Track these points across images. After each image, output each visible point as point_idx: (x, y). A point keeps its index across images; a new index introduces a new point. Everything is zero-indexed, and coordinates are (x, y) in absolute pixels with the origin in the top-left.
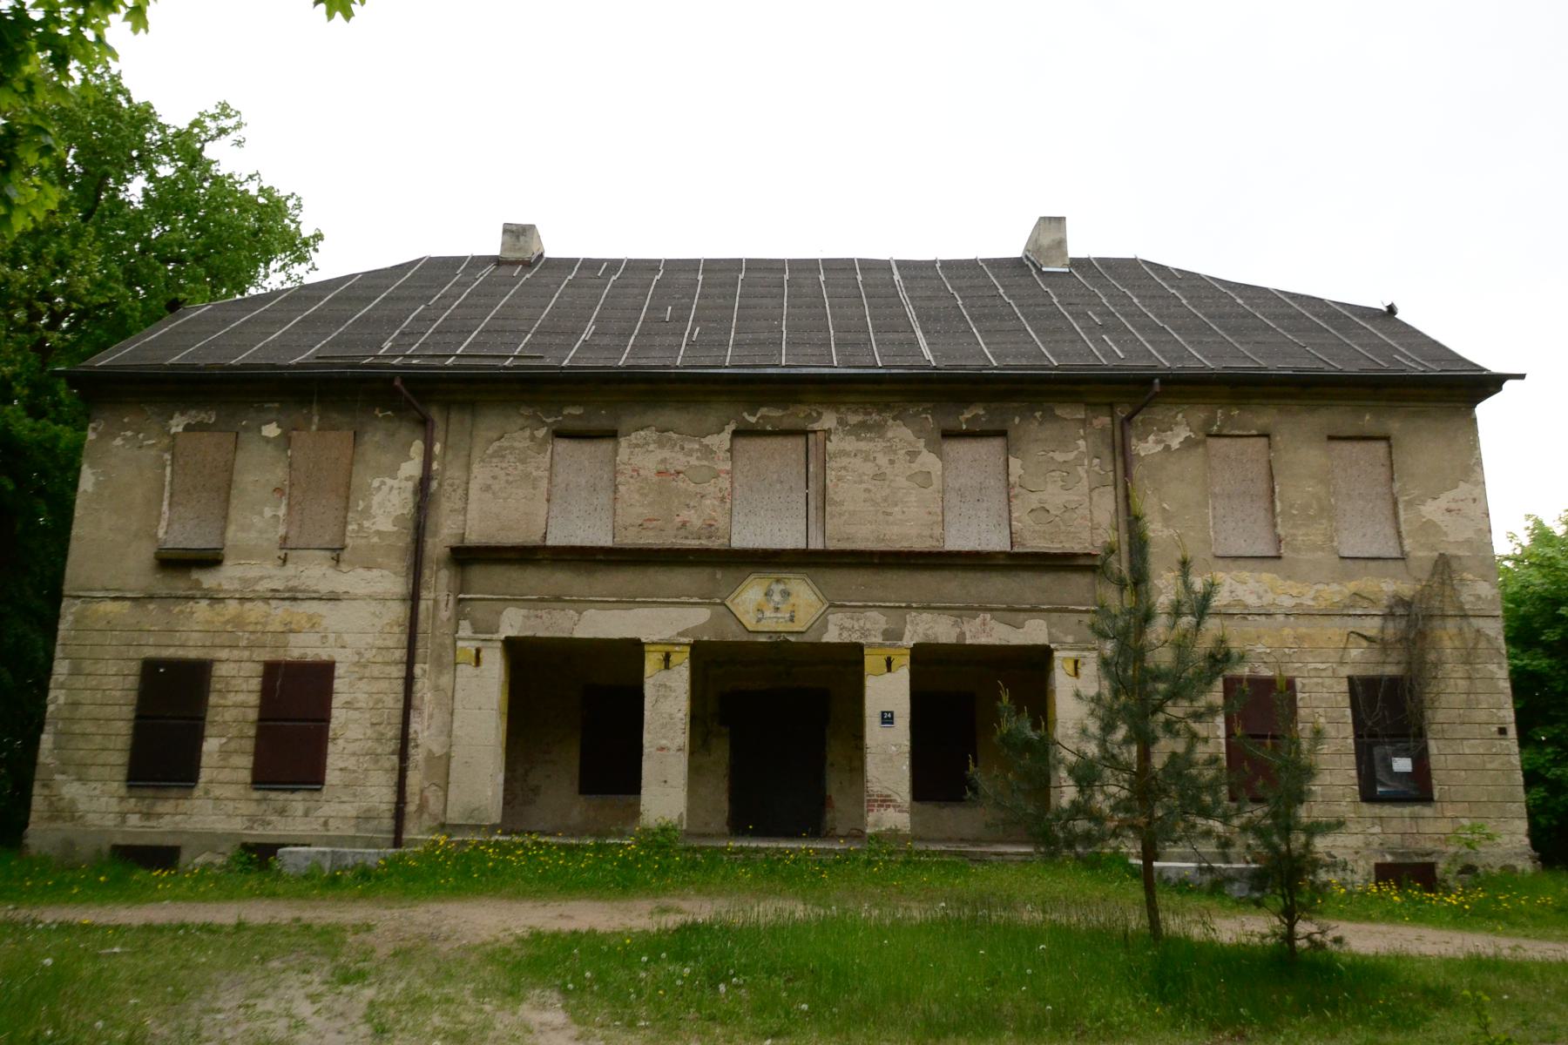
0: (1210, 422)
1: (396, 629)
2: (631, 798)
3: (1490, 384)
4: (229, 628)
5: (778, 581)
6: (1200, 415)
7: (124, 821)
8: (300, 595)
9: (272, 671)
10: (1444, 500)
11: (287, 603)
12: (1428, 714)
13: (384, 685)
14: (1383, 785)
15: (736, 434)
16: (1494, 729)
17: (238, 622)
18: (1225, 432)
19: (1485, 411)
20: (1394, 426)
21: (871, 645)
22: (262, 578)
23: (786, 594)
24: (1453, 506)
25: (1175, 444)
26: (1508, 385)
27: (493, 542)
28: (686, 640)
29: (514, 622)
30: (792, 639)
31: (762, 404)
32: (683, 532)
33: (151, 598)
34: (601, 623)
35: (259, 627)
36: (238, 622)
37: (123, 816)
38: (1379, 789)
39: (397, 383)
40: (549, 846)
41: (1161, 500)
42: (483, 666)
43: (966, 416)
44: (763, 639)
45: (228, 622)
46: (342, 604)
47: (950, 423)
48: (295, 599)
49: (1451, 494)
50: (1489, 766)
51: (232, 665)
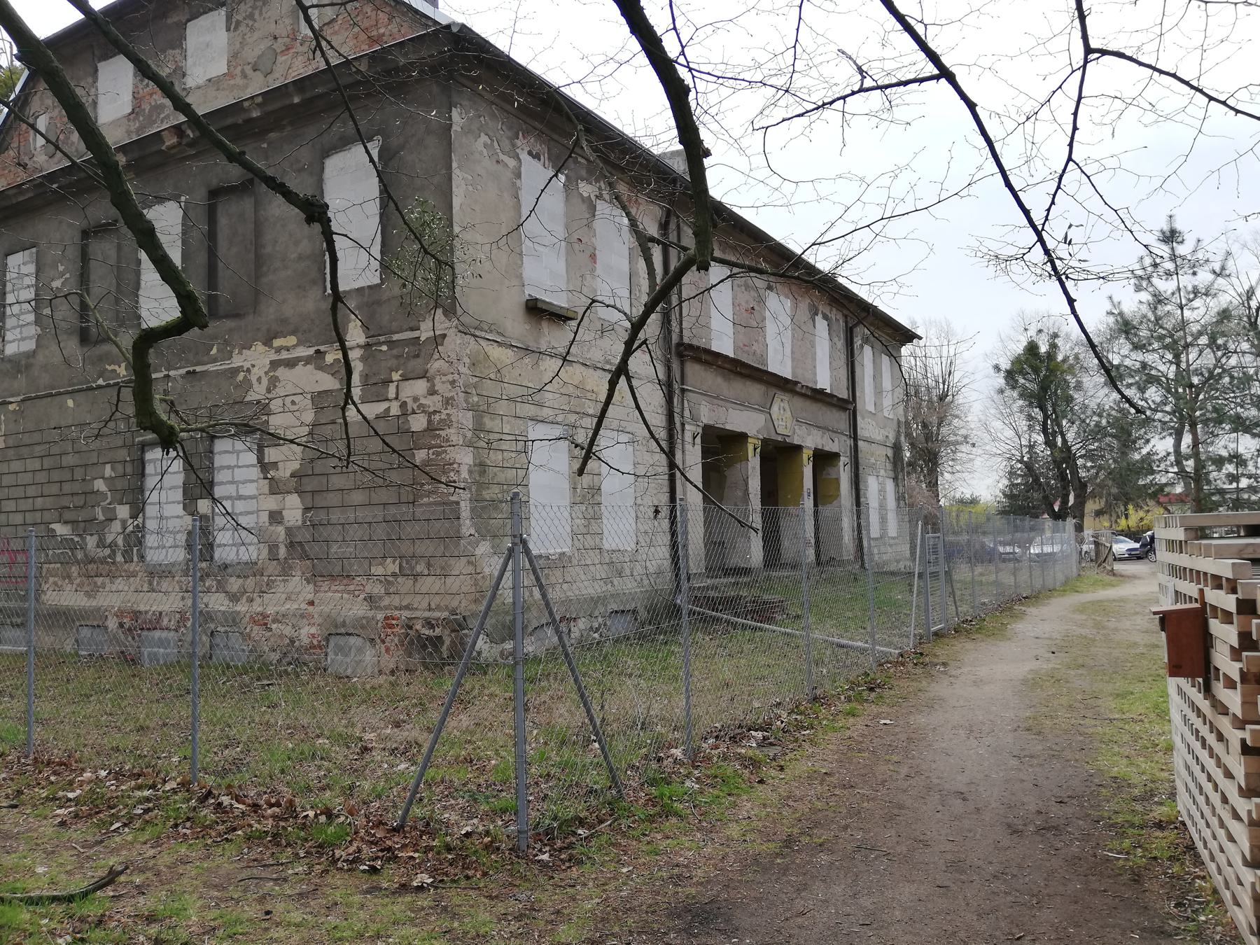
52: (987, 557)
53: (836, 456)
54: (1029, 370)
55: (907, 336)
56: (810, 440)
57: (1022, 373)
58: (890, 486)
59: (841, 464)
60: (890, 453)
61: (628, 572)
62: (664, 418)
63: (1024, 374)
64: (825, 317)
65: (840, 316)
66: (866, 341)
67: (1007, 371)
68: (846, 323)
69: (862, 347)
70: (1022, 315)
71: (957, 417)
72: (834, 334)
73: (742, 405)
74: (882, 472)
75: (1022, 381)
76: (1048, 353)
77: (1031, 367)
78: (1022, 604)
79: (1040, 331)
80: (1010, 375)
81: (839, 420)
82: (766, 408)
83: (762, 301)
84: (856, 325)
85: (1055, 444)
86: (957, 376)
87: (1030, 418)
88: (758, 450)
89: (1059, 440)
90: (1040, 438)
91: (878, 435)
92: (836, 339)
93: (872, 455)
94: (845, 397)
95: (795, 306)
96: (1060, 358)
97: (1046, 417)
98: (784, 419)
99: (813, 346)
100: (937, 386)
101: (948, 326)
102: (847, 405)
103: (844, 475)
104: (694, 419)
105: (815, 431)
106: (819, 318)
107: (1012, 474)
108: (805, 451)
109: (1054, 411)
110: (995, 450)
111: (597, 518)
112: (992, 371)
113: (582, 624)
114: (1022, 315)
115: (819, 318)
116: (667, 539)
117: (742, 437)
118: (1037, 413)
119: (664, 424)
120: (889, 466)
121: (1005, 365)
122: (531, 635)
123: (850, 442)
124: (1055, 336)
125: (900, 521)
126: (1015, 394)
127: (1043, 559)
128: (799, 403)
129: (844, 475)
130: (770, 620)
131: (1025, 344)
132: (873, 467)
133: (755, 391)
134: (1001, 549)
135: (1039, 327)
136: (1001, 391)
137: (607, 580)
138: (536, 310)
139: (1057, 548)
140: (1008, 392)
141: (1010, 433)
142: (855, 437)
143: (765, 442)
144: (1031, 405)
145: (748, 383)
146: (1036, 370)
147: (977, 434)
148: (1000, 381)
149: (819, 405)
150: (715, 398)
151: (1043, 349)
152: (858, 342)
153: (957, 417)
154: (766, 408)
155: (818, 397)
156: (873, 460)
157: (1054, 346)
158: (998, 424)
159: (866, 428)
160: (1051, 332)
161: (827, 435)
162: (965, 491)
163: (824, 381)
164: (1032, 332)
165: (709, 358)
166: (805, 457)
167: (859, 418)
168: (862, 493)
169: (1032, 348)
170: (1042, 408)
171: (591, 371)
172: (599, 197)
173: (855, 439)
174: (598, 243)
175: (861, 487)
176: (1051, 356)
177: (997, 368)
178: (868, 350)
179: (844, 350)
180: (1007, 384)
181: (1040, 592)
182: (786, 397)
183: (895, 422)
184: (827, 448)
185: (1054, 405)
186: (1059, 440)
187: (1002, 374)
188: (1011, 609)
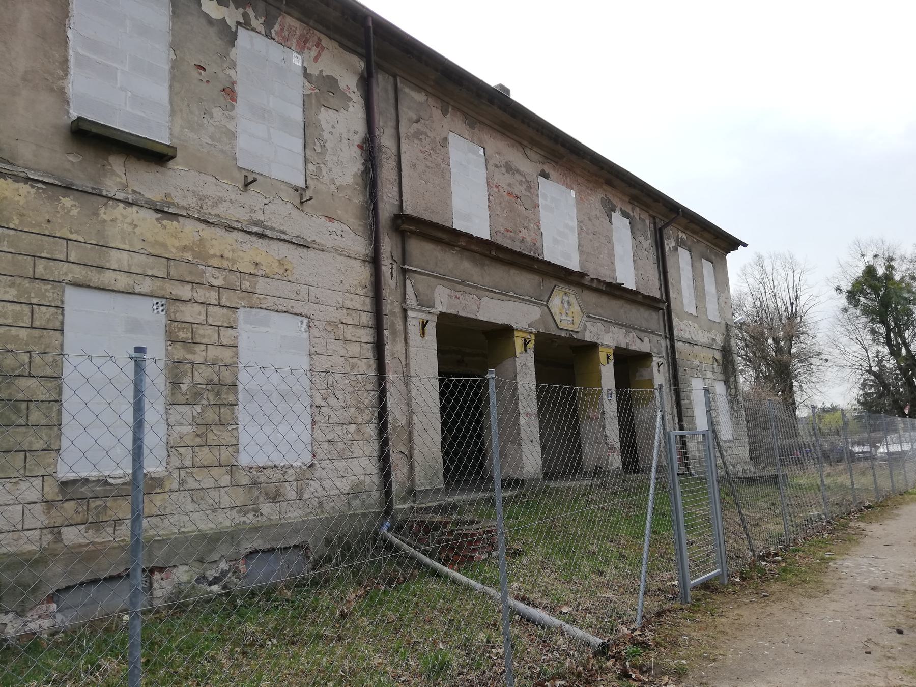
1: (360, 291)
3: (733, 244)
4: (188, 256)
7: (58, 537)
8: (268, 233)
11: (254, 238)
12: (362, 168)
13: (354, 349)
17: (200, 252)
19: (731, 257)
22: (221, 200)
26: (741, 247)
27: (427, 216)
28: (534, 330)
29: (444, 301)
33: (68, 188)
34: (493, 311)
35: (225, 264)
36: (200, 252)
37: (55, 530)
40: (552, 610)
42: (426, 338)
43: (692, 226)
44: (563, 334)
45: (185, 248)
46: (311, 253)
48: (262, 236)
51: (198, 308)
52: (834, 456)
53: (647, 357)
54: (869, 291)
55: (733, 244)
56: (609, 338)
57: (862, 291)
58: (720, 389)
59: (654, 365)
60: (718, 356)
61: (291, 494)
62: (368, 301)
63: (865, 295)
64: (625, 215)
65: (645, 216)
66: (680, 243)
67: (848, 292)
68: (655, 224)
69: (675, 249)
70: (858, 242)
71: (804, 333)
72: (638, 233)
73: (504, 294)
74: (709, 375)
75: (862, 299)
76: (885, 274)
77: (870, 286)
78: (862, 519)
79: (876, 256)
80: (852, 296)
81: (654, 320)
82: (543, 301)
83: (531, 187)
84: (666, 225)
85: (900, 354)
86: (803, 299)
87: (873, 332)
88: (531, 345)
89: (904, 352)
90: (885, 350)
91: (703, 337)
92: (642, 239)
93: (696, 357)
94: (658, 296)
95: (579, 201)
96: (897, 278)
97: (889, 331)
98: (568, 313)
99: (610, 241)
100: (787, 309)
101: (792, 258)
102: (659, 305)
103: (660, 376)
104: (425, 303)
105: (616, 329)
106: (616, 216)
107: (864, 385)
108: (601, 349)
109: (896, 325)
110: (845, 362)
111: (228, 424)
112: (834, 292)
113: (182, 574)
114: (858, 242)
115: (616, 216)
116: (373, 448)
117: (505, 332)
118: (882, 329)
119: (369, 307)
120: (717, 369)
121: (847, 286)
122: (51, 599)
123: (664, 343)
124: (891, 259)
125: (736, 425)
126: (858, 312)
127: (894, 459)
128: (592, 298)
129: (660, 376)
130: (465, 561)
131: (863, 268)
132: (697, 369)
133: (525, 281)
134: (857, 449)
135: (875, 253)
136: (845, 310)
137: (242, 509)
138: (92, 139)
139: (906, 447)
140: (852, 310)
141: (857, 347)
142: (670, 336)
143: (538, 335)
144: (873, 320)
145: (513, 271)
146: (876, 290)
147: (829, 351)
148: (843, 301)
149: (620, 303)
150: (459, 283)
151: (881, 271)
152: (669, 244)
153: (804, 333)
154: (543, 301)
155: (618, 293)
156: (696, 362)
157: (890, 267)
158: (845, 340)
159: (683, 328)
160: (887, 255)
161: (633, 334)
162: (821, 401)
163: (627, 277)
164: (869, 257)
165: (444, 236)
166: (602, 356)
167: (675, 320)
168: (683, 395)
169: (870, 271)
170: (884, 322)
171: (219, 232)
172: (246, 24)
173: (672, 339)
174: (238, 75)
175: (682, 387)
176: (888, 277)
177: (839, 289)
178: (684, 256)
179: (652, 250)
180: (850, 302)
181: (888, 498)
182: (572, 291)
183: (723, 326)
184: (633, 347)
185: (896, 320)
186: (904, 352)
187: (844, 295)
188: (845, 526)
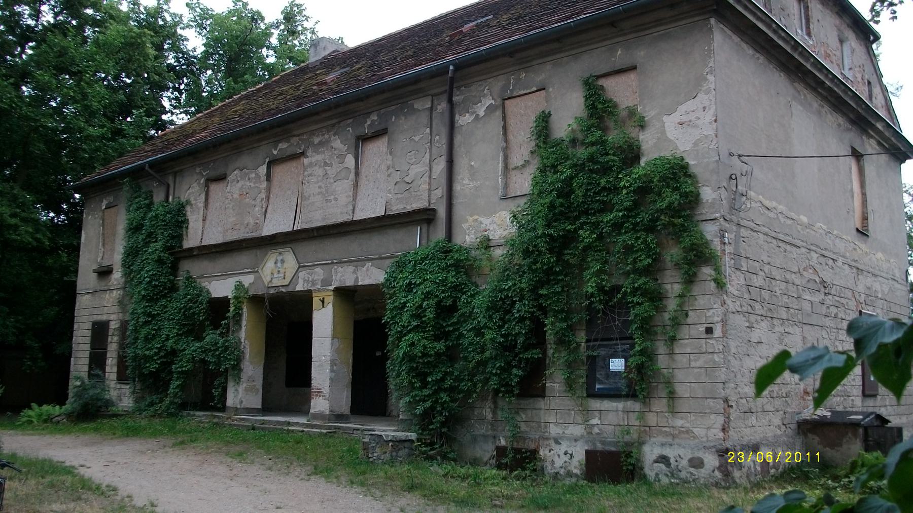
0: (505, 88)
2: (306, 389)
5: (280, 254)
6: (497, 84)
9: (95, 324)
10: (676, 117)
14: (601, 382)
15: (270, 164)
16: (702, 329)
18: (515, 94)
20: (640, 55)
21: (315, 290)
23: (283, 261)
24: (684, 118)
25: (482, 113)
30: (284, 290)
31: (279, 141)
32: (247, 230)
38: (597, 386)
39: (147, 168)
41: (470, 160)
47: (359, 132)
49: (690, 105)
50: (693, 364)
